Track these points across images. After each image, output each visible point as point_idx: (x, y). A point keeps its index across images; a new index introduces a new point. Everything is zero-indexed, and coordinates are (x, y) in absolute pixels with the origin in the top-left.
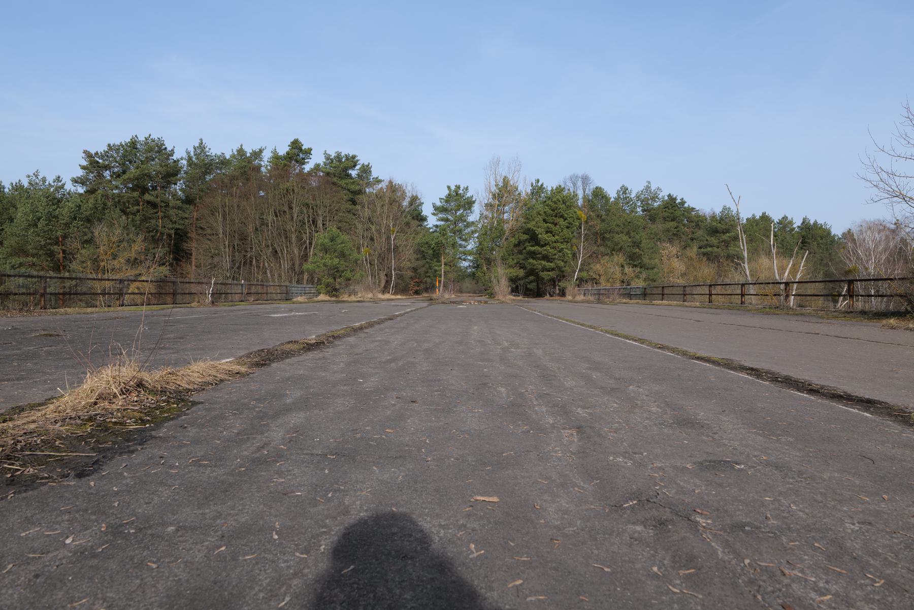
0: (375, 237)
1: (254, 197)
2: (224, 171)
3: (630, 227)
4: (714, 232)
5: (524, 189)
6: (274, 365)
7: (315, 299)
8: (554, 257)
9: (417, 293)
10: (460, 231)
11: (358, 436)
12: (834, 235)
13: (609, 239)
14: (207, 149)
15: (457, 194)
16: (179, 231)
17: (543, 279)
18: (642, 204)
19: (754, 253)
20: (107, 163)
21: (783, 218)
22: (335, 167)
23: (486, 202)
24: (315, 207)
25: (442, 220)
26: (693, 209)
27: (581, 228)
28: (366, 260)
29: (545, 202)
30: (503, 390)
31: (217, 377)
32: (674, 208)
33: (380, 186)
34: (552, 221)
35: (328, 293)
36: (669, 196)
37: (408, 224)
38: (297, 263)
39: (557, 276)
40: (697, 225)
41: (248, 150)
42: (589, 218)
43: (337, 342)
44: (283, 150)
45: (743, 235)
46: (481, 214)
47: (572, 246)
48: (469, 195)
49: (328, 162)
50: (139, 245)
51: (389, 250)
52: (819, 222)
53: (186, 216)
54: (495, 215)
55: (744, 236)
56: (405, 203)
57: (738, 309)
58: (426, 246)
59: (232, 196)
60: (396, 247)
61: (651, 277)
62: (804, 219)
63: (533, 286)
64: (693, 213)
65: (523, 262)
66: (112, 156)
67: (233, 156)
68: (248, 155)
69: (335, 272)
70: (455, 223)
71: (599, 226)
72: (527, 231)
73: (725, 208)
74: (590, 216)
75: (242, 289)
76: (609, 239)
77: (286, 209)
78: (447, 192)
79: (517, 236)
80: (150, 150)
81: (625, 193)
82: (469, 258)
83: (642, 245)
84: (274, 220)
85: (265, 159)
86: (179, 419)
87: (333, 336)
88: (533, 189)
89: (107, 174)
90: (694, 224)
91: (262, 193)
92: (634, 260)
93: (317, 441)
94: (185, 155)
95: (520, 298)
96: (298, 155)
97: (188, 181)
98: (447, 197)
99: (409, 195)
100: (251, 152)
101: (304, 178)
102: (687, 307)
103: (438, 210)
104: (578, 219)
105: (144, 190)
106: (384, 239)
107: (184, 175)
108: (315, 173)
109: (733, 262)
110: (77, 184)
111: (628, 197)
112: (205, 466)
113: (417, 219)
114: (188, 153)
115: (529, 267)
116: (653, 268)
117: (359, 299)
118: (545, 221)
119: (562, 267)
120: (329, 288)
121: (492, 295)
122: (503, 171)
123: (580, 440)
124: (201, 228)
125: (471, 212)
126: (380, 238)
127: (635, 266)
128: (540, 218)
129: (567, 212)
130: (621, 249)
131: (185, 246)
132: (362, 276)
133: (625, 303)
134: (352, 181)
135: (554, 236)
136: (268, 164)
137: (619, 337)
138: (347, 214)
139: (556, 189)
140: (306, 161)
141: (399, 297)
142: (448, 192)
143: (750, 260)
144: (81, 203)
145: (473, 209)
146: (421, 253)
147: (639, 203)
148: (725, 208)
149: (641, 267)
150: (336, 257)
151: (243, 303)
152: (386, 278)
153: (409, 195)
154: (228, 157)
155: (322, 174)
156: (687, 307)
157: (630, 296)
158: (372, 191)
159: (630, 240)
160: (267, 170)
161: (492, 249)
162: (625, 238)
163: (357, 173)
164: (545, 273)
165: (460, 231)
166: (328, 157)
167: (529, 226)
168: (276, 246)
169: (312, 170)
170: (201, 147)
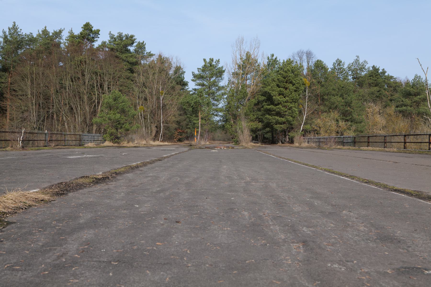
0: (148, 98)
1: (55, 67)
2: (32, 47)
4: (408, 94)
5: (262, 61)
6: (70, 194)
7: (102, 145)
8: (285, 113)
9: (180, 140)
10: (213, 93)
11: (135, 247)
13: (327, 100)
14: (19, 30)
17: (277, 130)
22: (118, 44)
23: (233, 71)
24: (102, 75)
25: (199, 85)
26: (392, 77)
27: (305, 91)
28: (141, 115)
29: (278, 71)
30: (246, 213)
31: (26, 203)
32: (377, 77)
33: (152, 59)
35: (112, 140)
36: (373, 67)
37: (173, 88)
39: (287, 128)
40: (395, 90)
41: (51, 31)
42: (312, 84)
43: (119, 177)
44: (77, 31)
46: (229, 81)
47: (299, 105)
48: (220, 66)
49: (112, 40)
54: (240, 81)
56: (171, 72)
57: (426, 154)
58: (187, 105)
61: (359, 129)
63: (269, 135)
64: (392, 80)
65: (261, 117)
67: (39, 35)
68: (51, 34)
69: (117, 125)
70: (209, 87)
71: (319, 90)
72: (265, 94)
73: (416, 76)
74: (312, 82)
75: (46, 137)
76: (327, 100)
77: (80, 76)
78: (203, 64)
79: (256, 98)
81: (339, 64)
82: (220, 114)
83: (352, 105)
84: (70, 84)
85: (64, 38)
87: (116, 173)
88: (269, 62)
90: (392, 89)
91: (61, 64)
93: (103, 251)
95: (259, 144)
96: (89, 35)
97: (4, 54)
98: (203, 67)
99: (174, 65)
100: (53, 32)
101: (93, 52)
102: (387, 152)
103: (196, 77)
104: (304, 84)
106: (155, 100)
108: (102, 48)
109: (422, 117)
111: (342, 68)
112: (17, 270)
113: (180, 84)
114: (4, 32)
115: (266, 121)
116: (361, 122)
117: (135, 145)
118: (278, 85)
119: (291, 121)
120: (112, 137)
121: (237, 142)
122: (246, 48)
123: (305, 251)
124: (14, 90)
125: (222, 79)
126: (152, 98)
127: (347, 120)
128: (274, 84)
130: (336, 107)
132: (138, 127)
133: (339, 149)
134: (130, 55)
135: (285, 97)
136: (66, 41)
137: (335, 174)
138: (127, 80)
139: (286, 62)
140: (95, 39)
141: (166, 143)
146: (183, 110)
148: (416, 76)
149: (352, 122)
151: (46, 148)
152: (156, 128)
153: (174, 65)
154: (35, 36)
155: (107, 49)
156: (387, 152)
157: (343, 143)
159: (343, 101)
160: (65, 46)
161: (238, 107)
162: (340, 99)
164: (278, 125)
165: (213, 93)
166: (112, 37)
167: (266, 89)
168: (72, 104)
169: (100, 46)
170: (14, 28)
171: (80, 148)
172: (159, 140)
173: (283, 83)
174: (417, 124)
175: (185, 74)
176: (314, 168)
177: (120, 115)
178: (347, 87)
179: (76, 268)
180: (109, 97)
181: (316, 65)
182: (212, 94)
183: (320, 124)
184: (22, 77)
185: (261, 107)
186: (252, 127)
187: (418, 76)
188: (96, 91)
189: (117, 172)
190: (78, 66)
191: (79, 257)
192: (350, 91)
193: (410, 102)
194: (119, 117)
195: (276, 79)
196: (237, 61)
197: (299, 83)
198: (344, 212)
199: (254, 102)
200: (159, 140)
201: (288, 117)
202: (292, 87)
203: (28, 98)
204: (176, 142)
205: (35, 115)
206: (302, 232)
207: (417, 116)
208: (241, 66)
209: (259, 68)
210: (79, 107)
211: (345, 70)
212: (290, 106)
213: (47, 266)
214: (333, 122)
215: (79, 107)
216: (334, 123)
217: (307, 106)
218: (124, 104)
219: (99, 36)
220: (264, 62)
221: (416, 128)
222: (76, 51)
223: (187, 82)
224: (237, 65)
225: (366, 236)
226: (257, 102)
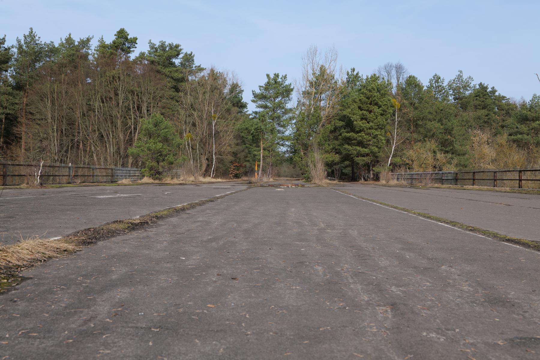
0: (197, 123)
1: (82, 84)
2: (53, 59)
4: (524, 120)
6: (100, 243)
7: (139, 181)
8: (368, 143)
9: (237, 176)
10: (279, 117)
11: (181, 310)
14: (37, 38)
15: (276, 82)
16: (9, 116)
17: (358, 164)
22: (159, 56)
23: (304, 90)
26: (503, 97)
27: (394, 115)
28: (188, 145)
29: (360, 90)
31: (45, 254)
32: (485, 97)
33: (202, 74)
34: (367, 108)
35: (152, 176)
36: (480, 85)
37: (228, 111)
38: (122, 147)
39: (372, 161)
42: (403, 106)
44: (110, 39)
46: (299, 102)
47: (386, 132)
48: (287, 83)
49: (152, 51)
53: (17, 101)
54: (312, 103)
56: (226, 91)
58: (246, 131)
59: (60, 83)
60: (217, 133)
61: (462, 163)
63: (348, 171)
64: (504, 101)
65: (339, 147)
67: (62, 45)
68: (76, 43)
69: (159, 156)
70: (274, 110)
71: (412, 114)
72: (343, 118)
74: (403, 104)
75: (69, 172)
77: (112, 95)
78: (266, 80)
79: (333, 123)
81: (437, 81)
82: (287, 143)
83: (453, 132)
84: (100, 106)
86: (10, 293)
87: (156, 216)
88: (349, 78)
91: (89, 80)
93: (141, 315)
94: (15, 43)
96: (124, 44)
98: (266, 85)
99: (230, 82)
100: (79, 40)
101: (129, 65)
102: (497, 191)
103: (257, 97)
104: (392, 106)
106: (205, 125)
107: (15, 63)
108: (140, 61)
111: (441, 86)
112: (34, 337)
113: (238, 106)
114: (19, 41)
115: (344, 152)
116: (464, 155)
117: (181, 182)
118: (360, 108)
119: (376, 153)
120: (152, 171)
121: (308, 179)
122: (320, 61)
123: (394, 317)
124: (31, 113)
125: (289, 100)
126: (202, 123)
127: (447, 152)
128: (355, 106)
129: (382, 100)
130: (433, 136)
131: (15, 130)
132: (184, 160)
133: (437, 188)
134: (175, 69)
135: (368, 123)
136: (95, 52)
138: (170, 100)
139: (371, 78)
140: (131, 49)
141: (220, 180)
145: (291, 96)
146: (240, 139)
149: (453, 153)
150: (160, 142)
151: (70, 185)
152: (207, 161)
153: (230, 82)
154: (57, 45)
155: (146, 62)
156: (497, 191)
157: (442, 181)
158: (194, 78)
159: (442, 127)
160: (95, 58)
161: (309, 135)
162: (438, 125)
164: (360, 158)
165: (279, 117)
166: (152, 46)
167: (345, 113)
168: (102, 131)
169: (137, 58)
170: (31, 36)
171: (112, 186)
172: (210, 176)
173: (367, 104)
174: (535, 157)
175: (243, 93)
176: (405, 211)
177: (161, 144)
178: (448, 110)
179: (107, 335)
180: (149, 122)
181: (408, 82)
182: (277, 118)
183: (413, 156)
184: (41, 96)
185: (339, 134)
186: (327, 160)
187: (537, 95)
188: (132, 114)
189: (159, 216)
190: (110, 83)
191: (111, 321)
192: (451, 114)
193: (527, 129)
194: (161, 147)
195: (357, 100)
196: (309, 77)
197: (386, 105)
198: (443, 267)
199: (330, 128)
200: (210, 176)
201: (373, 148)
202: (378, 110)
203: (47, 122)
204: (232, 179)
205: (56, 144)
206: (390, 292)
207: (536, 147)
208: (314, 83)
209: (336, 86)
210: (111, 135)
211: (444, 89)
212: (375, 134)
213: (72, 332)
214: (429, 154)
215: (111, 135)
216: (430, 155)
217: (396, 134)
218: (167, 130)
219: (136, 45)
220: (343, 78)
221: (535, 162)
222: (108, 64)
223: (246, 103)
224: (308, 82)
225: (471, 298)
226: (334, 128)
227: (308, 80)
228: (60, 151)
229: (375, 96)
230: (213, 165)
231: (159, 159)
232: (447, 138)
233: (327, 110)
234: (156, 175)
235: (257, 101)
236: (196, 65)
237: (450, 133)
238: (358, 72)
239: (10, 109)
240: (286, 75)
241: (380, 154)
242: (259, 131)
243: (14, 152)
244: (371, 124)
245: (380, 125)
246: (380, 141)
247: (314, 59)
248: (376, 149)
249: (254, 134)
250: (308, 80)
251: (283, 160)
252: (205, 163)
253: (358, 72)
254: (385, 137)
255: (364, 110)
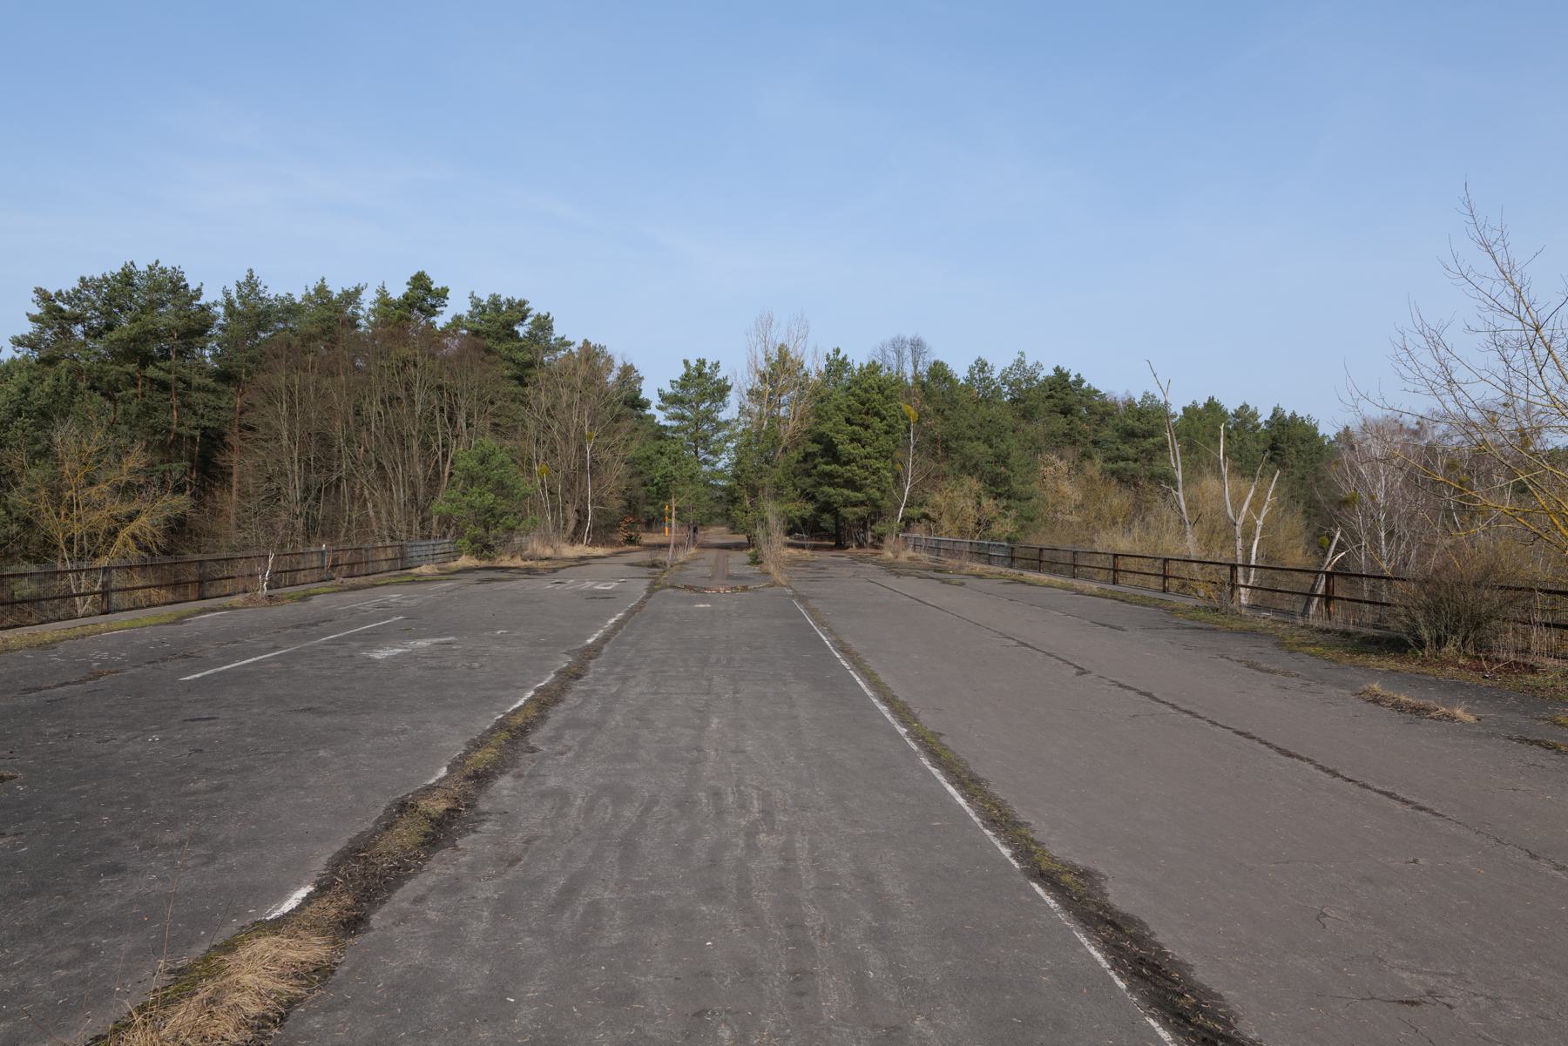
3: (990, 432)
4: (1129, 435)
7: (453, 565)
8: (864, 482)
12: (1324, 436)
13: (956, 451)
14: (261, 288)
18: (1010, 388)
19: (1194, 470)
20: (78, 311)
21: (1242, 407)
22: (489, 321)
23: (750, 388)
26: (1096, 391)
29: (850, 388)
34: (860, 422)
35: (477, 553)
39: (869, 514)
41: (336, 290)
44: (398, 291)
45: (1176, 444)
46: (742, 408)
48: (720, 376)
50: (136, 459)
51: (582, 467)
52: (1299, 415)
53: (223, 404)
55: (1177, 447)
59: (305, 370)
62: (1275, 410)
66: (88, 299)
67: (308, 298)
68: (335, 296)
69: (488, 518)
70: (697, 424)
71: (939, 429)
72: (820, 438)
75: (323, 561)
76: (956, 451)
77: (401, 393)
78: (683, 371)
80: (159, 288)
81: (982, 370)
83: (1010, 461)
88: (830, 365)
89: (78, 330)
92: (998, 486)
94: (220, 298)
96: (424, 299)
98: (683, 379)
99: (618, 363)
101: (433, 338)
104: (905, 418)
105: (146, 360)
106: (573, 450)
110: (21, 348)
111: (988, 378)
114: (227, 293)
116: (1029, 499)
118: (848, 421)
120: (476, 545)
122: (778, 337)
124: (250, 429)
125: (724, 406)
128: (840, 418)
129: (887, 406)
130: (975, 466)
135: (863, 447)
139: (867, 368)
140: (438, 309)
142: (685, 370)
143: (1186, 482)
144: (30, 385)
145: (727, 399)
147: (1006, 389)
148: (1146, 396)
149: (1009, 497)
150: (491, 491)
152: (576, 515)
153: (618, 363)
154: (298, 300)
162: (983, 448)
163: (527, 330)
164: (850, 509)
165: (705, 439)
166: (476, 303)
167: (822, 429)
169: (449, 326)
170: (251, 283)
187: (1150, 394)
192: (1006, 429)
195: (843, 407)
197: (893, 415)
200: (582, 543)
203: (281, 445)
204: (622, 546)
208: (768, 376)
211: (994, 384)
212: (875, 467)
223: (647, 400)
224: (757, 375)
227: (757, 371)
228: (306, 498)
229: (874, 400)
230: (586, 524)
231: (488, 522)
232: (998, 471)
233: (792, 424)
234: (483, 550)
235: (666, 408)
236: (557, 336)
237: (1004, 462)
238: (846, 356)
239: (209, 420)
240: (718, 363)
241: (884, 502)
242: (668, 479)
243: (218, 500)
244: (868, 449)
245: (883, 451)
246: (883, 479)
247: (768, 335)
248: (878, 494)
249: (660, 485)
250: (757, 371)
251: (714, 514)
252: (573, 517)
253: (846, 356)
254: (892, 470)
255: (857, 425)
